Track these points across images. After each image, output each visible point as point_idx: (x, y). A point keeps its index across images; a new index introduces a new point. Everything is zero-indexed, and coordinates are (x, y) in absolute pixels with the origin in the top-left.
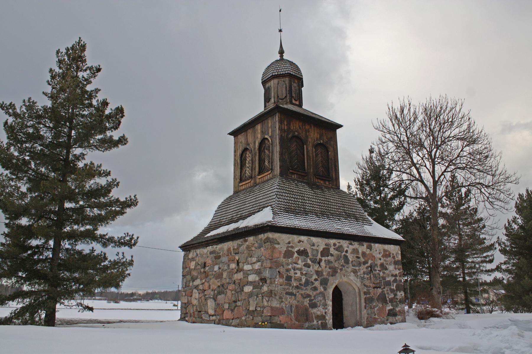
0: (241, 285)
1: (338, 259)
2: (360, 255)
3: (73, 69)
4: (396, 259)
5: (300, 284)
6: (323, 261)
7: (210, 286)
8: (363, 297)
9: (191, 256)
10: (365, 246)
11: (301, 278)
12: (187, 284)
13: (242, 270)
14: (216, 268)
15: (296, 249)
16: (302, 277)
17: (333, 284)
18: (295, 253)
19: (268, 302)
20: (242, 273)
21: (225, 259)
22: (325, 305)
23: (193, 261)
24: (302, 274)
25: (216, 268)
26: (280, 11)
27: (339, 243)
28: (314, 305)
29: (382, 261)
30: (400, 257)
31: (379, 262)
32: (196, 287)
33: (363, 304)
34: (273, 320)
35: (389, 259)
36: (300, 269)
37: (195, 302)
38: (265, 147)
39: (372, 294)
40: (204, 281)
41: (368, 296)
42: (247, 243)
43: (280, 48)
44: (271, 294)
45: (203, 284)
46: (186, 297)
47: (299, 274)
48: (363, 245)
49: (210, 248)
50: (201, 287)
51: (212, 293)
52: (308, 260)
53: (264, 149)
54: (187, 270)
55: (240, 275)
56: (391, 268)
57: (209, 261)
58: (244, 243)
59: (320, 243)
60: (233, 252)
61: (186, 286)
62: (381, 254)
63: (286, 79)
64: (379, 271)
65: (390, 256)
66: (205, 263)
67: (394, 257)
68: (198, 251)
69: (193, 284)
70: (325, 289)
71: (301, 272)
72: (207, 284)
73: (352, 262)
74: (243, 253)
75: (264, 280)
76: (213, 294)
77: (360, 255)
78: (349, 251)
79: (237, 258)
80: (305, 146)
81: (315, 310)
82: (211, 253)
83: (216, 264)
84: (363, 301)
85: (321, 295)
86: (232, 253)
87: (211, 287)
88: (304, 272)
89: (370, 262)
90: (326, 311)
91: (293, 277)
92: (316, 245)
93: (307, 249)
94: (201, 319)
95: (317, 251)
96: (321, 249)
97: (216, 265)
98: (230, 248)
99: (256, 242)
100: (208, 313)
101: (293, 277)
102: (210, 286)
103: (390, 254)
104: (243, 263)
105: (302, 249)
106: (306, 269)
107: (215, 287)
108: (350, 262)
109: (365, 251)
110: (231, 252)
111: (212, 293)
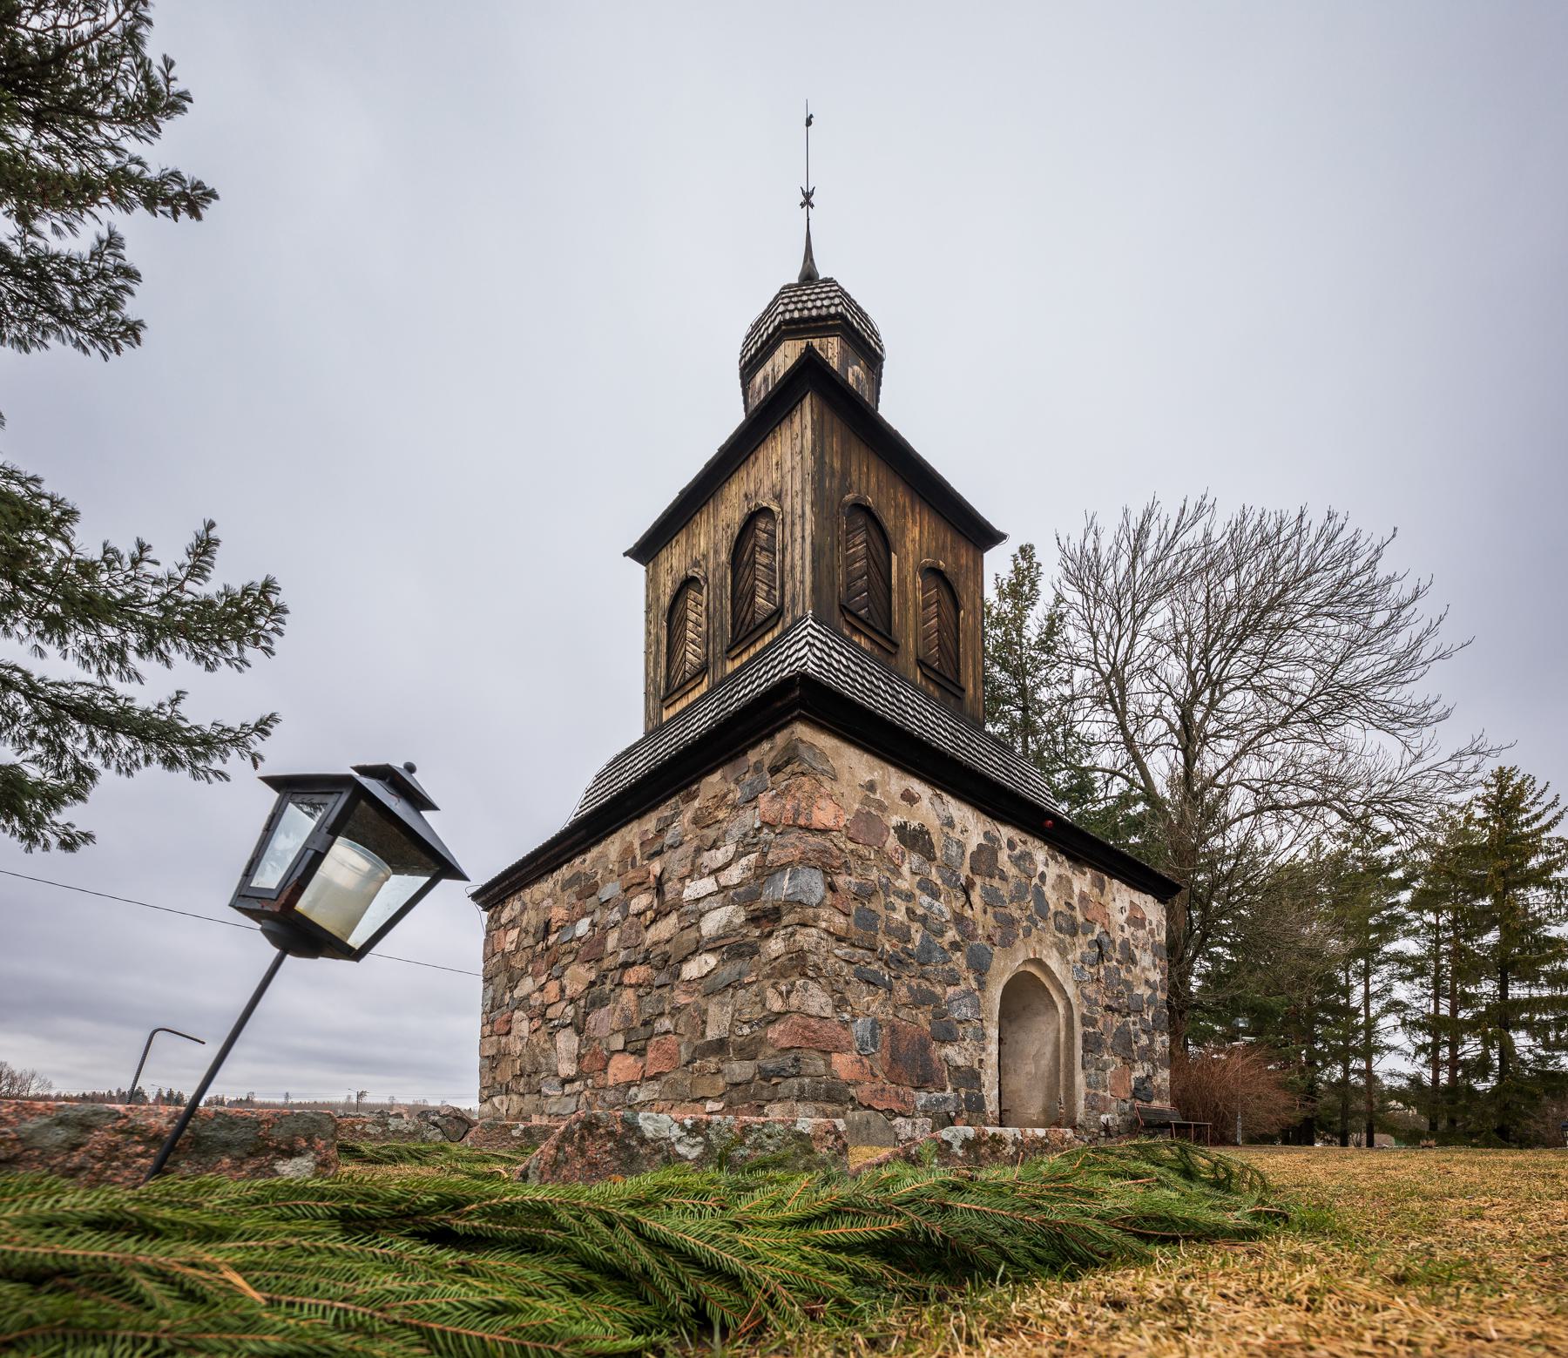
0: (668, 963)
1: (1019, 895)
2: (1075, 902)
3: (612, 1149)
4: (1157, 938)
5: (904, 950)
6: (978, 889)
7: (562, 990)
8: (1079, 1030)
9: (506, 916)
10: (1088, 875)
11: (909, 928)
12: (497, 1002)
13: (677, 906)
14: (583, 927)
15: (895, 820)
16: (912, 924)
17: (1002, 974)
18: (892, 831)
19: (788, 997)
20: (673, 918)
21: (610, 890)
22: (981, 1036)
23: (513, 928)
24: (910, 912)
25: (583, 927)
26: (809, 123)
27: (1025, 843)
28: (947, 1035)
29: (1127, 935)
30: (1164, 935)
31: (1118, 937)
32: (523, 1003)
33: (1079, 1053)
34: (807, 1064)
35: (1141, 933)
36: (909, 897)
37: (518, 1047)
38: (755, 545)
39: (1100, 1024)
40: (543, 979)
41: (1091, 1030)
42: (696, 804)
43: (805, 261)
44: (798, 962)
45: (541, 989)
46: (495, 1038)
47: (900, 916)
48: (1085, 874)
49: (565, 872)
50: (536, 1000)
51: (570, 1011)
52: (934, 870)
53: (753, 552)
54: (495, 960)
55: (666, 927)
56: (1145, 959)
57: (559, 913)
58: (682, 807)
59: (972, 826)
60: (642, 854)
61: (492, 1006)
62: (1126, 915)
63: (830, 339)
64: (1117, 961)
65: (1143, 927)
66: (548, 924)
67: (1151, 932)
68: (527, 895)
69: (511, 997)
70: (982, 986)
71: (907, 909)
72: (553, 987)
73: (1056, 914)
74: (681, 844)
75: (766, 918)
76: (572, 1013)
77: (1075, 902)
78: (1050, 880)
79: (656, 867)
80: (894, 557)
81: (950, 1051)
82: (567, 884)
83: (585, 914)
84: (1079, 1042)
85: (967, 1000)
86: (638, 858)
87: (568, 992)
88: (920, 911)
89: (1098, 929)
90: (983, 1057)
91: (884, 917)
92: (958, 828)
93: (931, 831)
94: (537, 1096)
95: (961, 845)
96: (971, 847)
97: (583, 916)
98: (632, 843)
99: (732, 786)
100: (557, 1075)
101: (884, 917)
102: (562, 990)
103: (1144, 919)
104: (682, 879)
105: (914, 824)
106: (925, 900)
107: (581, 988)
108: (1050, 914)
109: (1086, 890)
110: (634, 857)
111: (570, 1011)
